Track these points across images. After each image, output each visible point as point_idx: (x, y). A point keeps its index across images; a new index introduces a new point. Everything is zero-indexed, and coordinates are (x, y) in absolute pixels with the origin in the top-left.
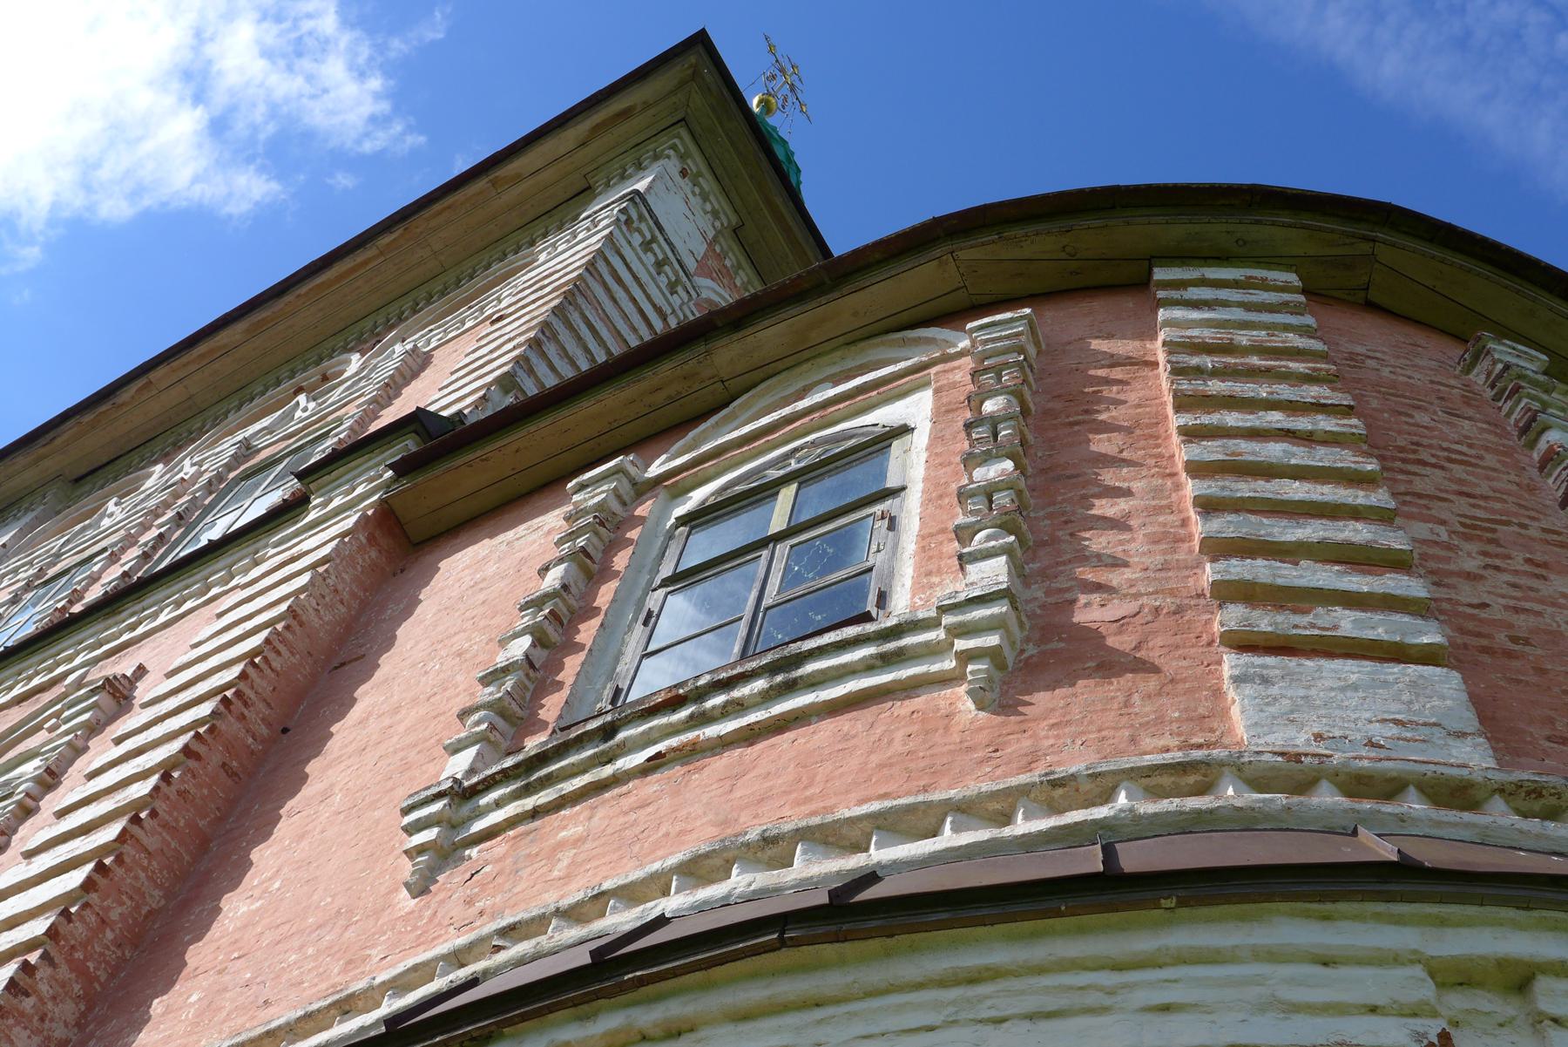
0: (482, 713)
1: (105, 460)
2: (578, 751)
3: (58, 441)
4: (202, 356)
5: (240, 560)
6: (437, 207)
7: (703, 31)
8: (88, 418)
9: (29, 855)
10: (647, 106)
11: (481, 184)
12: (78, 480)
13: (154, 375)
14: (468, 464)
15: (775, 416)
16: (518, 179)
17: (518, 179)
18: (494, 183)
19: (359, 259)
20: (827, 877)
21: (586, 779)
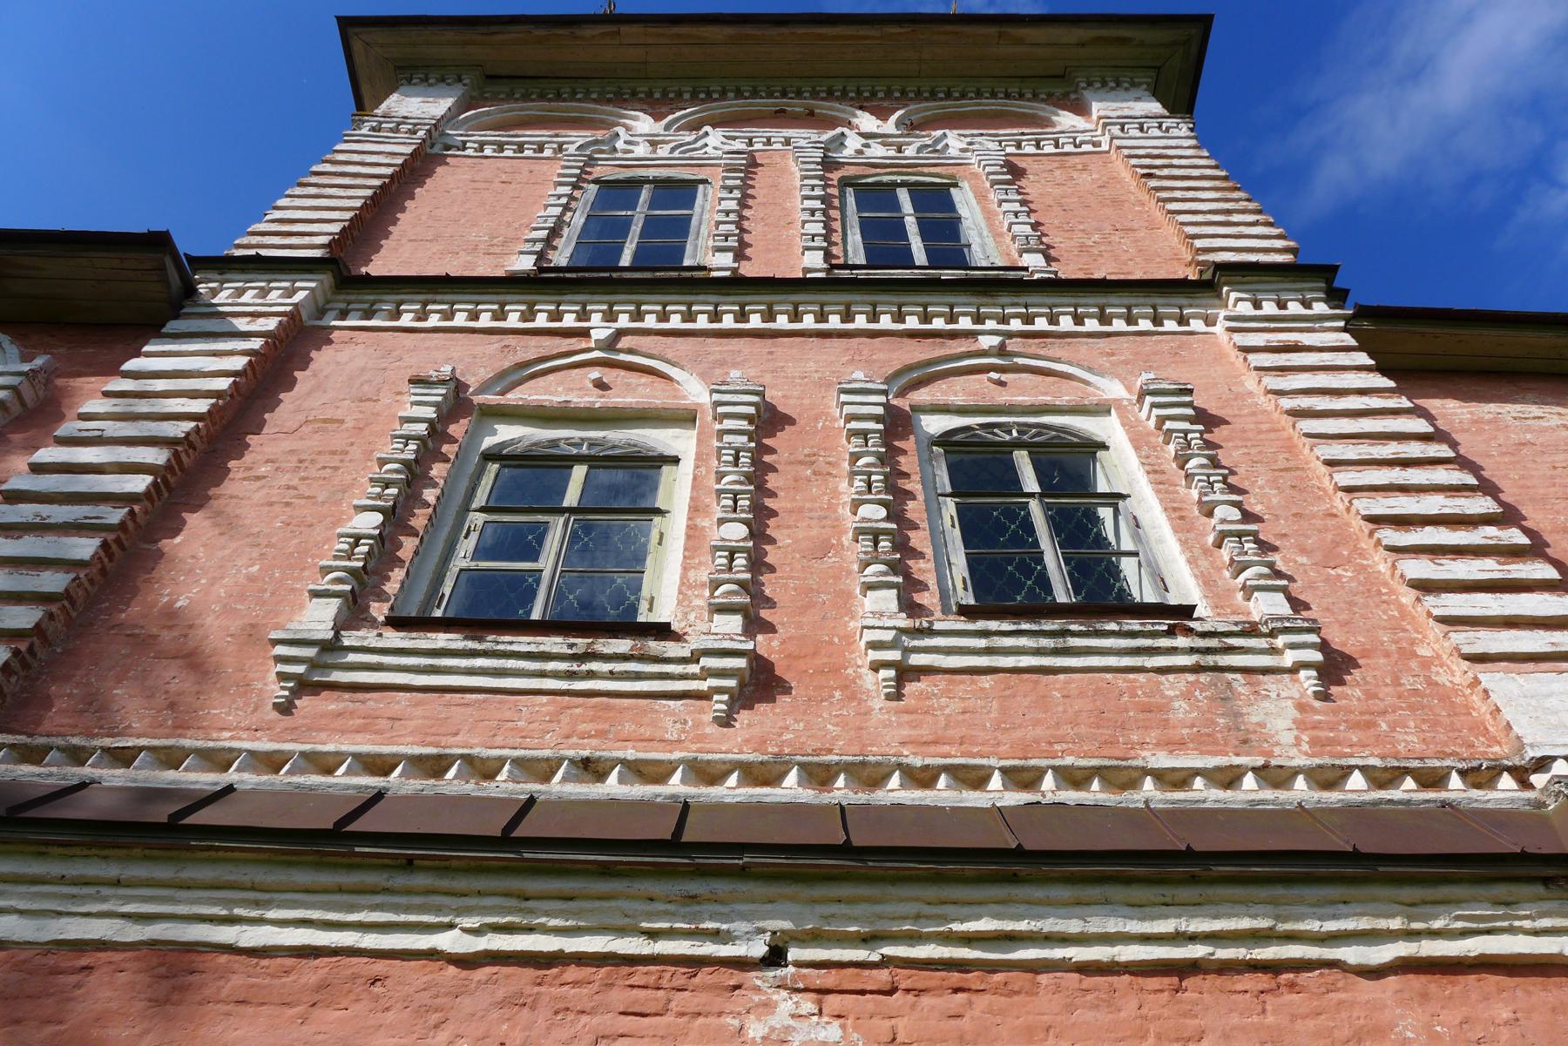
0: (396, 466)
1: (530, 73)
2: (1072, 873)
3: (499, 37)
4: (679, 36)
5: (1144, 305)
6: (948, 28)
7: (1212, 16)
8: (541, 32)
9: (38, 469)
10: (1142, 44)
11: (992, 30)
12: (492, 78)
13: (625, 29)
14: (1423, 334)
15: (595, 275)
16: (1020, 41)
17: (1020, 41)
18: (1000, 35)
19: (862, 33)
20: (358, 788)
21: (1058, 953)
